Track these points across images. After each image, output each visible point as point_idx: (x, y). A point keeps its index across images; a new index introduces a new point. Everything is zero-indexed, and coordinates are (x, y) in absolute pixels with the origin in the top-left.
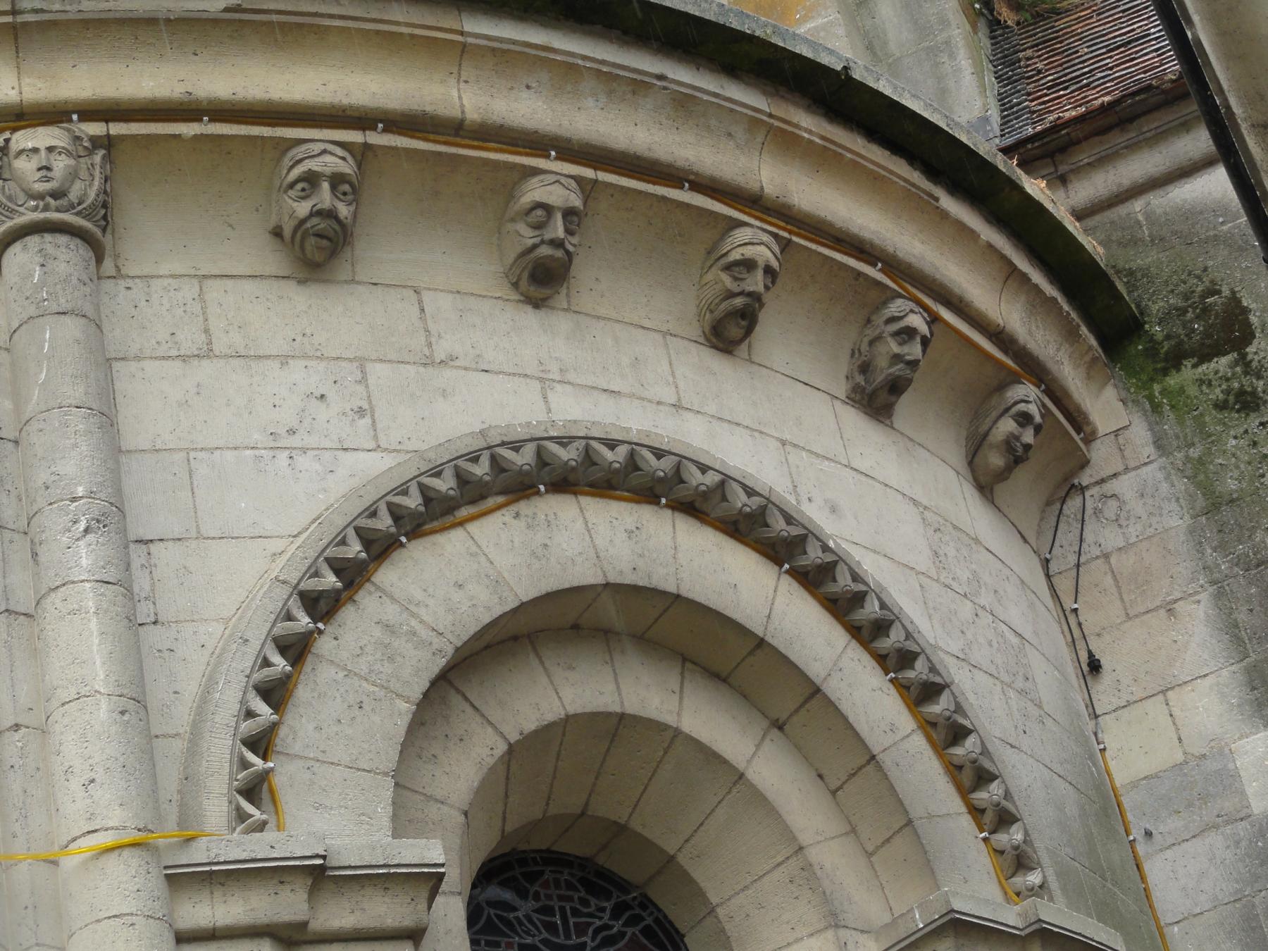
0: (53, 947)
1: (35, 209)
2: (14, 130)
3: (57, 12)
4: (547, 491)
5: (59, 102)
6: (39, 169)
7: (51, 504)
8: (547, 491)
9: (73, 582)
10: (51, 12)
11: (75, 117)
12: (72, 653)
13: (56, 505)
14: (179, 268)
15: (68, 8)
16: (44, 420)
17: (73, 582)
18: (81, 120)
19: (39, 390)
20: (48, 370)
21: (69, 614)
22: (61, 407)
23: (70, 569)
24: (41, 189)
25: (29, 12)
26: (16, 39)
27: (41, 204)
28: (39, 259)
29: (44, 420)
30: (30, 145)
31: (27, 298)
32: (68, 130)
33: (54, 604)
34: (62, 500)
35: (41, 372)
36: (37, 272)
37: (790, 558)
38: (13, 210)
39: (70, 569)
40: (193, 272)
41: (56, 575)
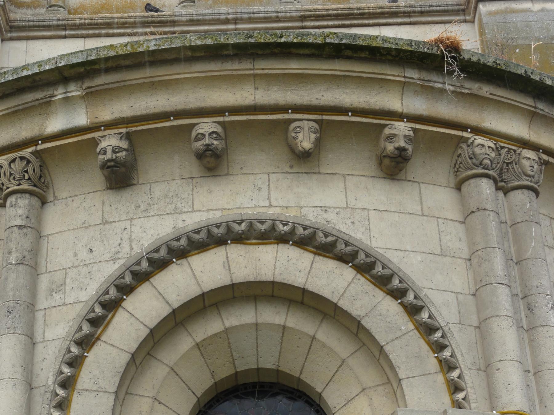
0: (177, 413)
1: (527, 180)
2: (524, 148)
3: (546, 112)
4: (231, 243)
5: (540, 144)
6: (531, 166)
7: (539, 294)
8: (231, 243)
9: (550, 326)
10: (545, 112)
11: (541, 151)
12: (551, 352)
13: (542, 295)
14: (545, 212)
15: (550, 112)
16: (535, 261)
17: (550, 326)
18: (543, 153)
19: (532, 250)
20: (535, 243)
21: (549, 337)
22: (540, 259)
23: (549, 320)
24: (531, 174)
25: (539, 109)
26: (402, 94)
27: (530, 179)
28: (528, 199)
29: (535, 261)
30: (528, 156)
31: (525, 213)
32: (537, 154)
33: (543, 331)
34: (543, 294)
35: (532, 243)
36: (528, 204)
37: (386, 285)
38: (521, 178)
39: (549, 320)
40: (548, 215)
41: (543, 321)
